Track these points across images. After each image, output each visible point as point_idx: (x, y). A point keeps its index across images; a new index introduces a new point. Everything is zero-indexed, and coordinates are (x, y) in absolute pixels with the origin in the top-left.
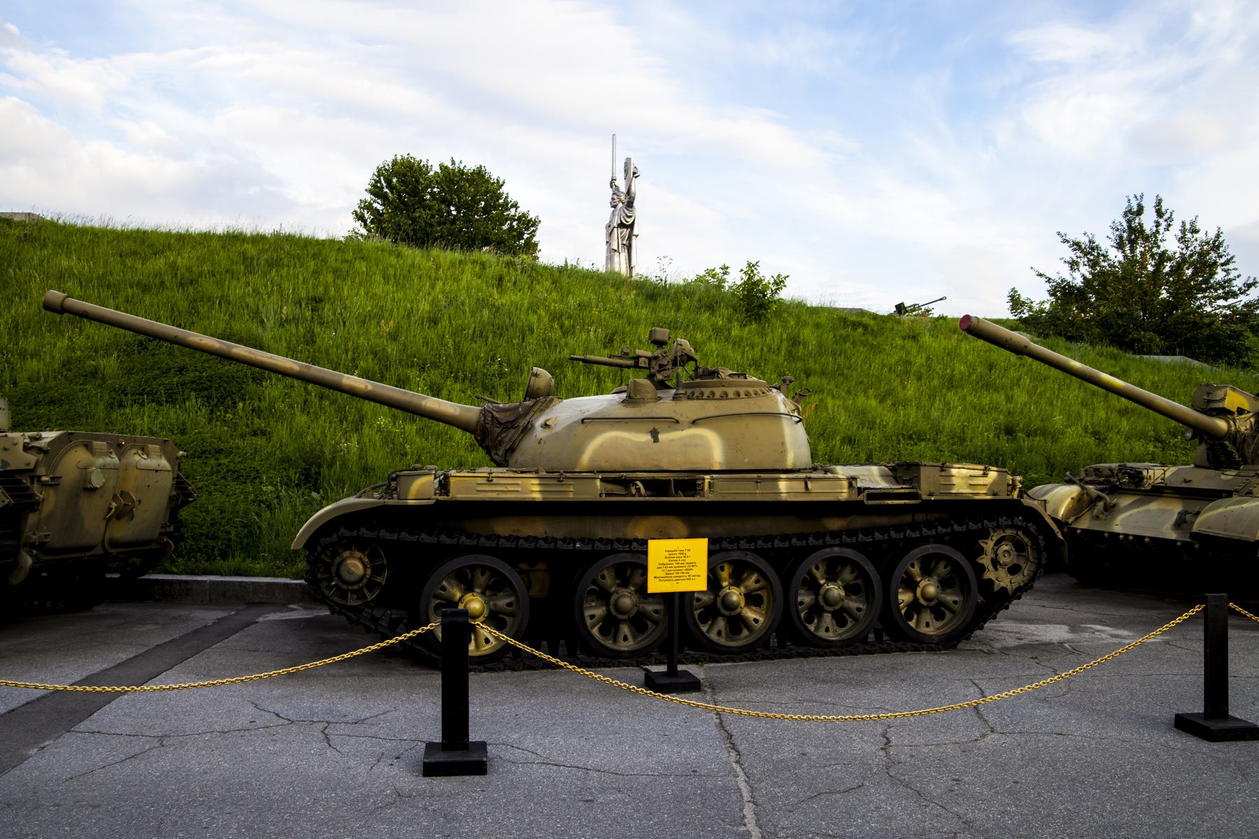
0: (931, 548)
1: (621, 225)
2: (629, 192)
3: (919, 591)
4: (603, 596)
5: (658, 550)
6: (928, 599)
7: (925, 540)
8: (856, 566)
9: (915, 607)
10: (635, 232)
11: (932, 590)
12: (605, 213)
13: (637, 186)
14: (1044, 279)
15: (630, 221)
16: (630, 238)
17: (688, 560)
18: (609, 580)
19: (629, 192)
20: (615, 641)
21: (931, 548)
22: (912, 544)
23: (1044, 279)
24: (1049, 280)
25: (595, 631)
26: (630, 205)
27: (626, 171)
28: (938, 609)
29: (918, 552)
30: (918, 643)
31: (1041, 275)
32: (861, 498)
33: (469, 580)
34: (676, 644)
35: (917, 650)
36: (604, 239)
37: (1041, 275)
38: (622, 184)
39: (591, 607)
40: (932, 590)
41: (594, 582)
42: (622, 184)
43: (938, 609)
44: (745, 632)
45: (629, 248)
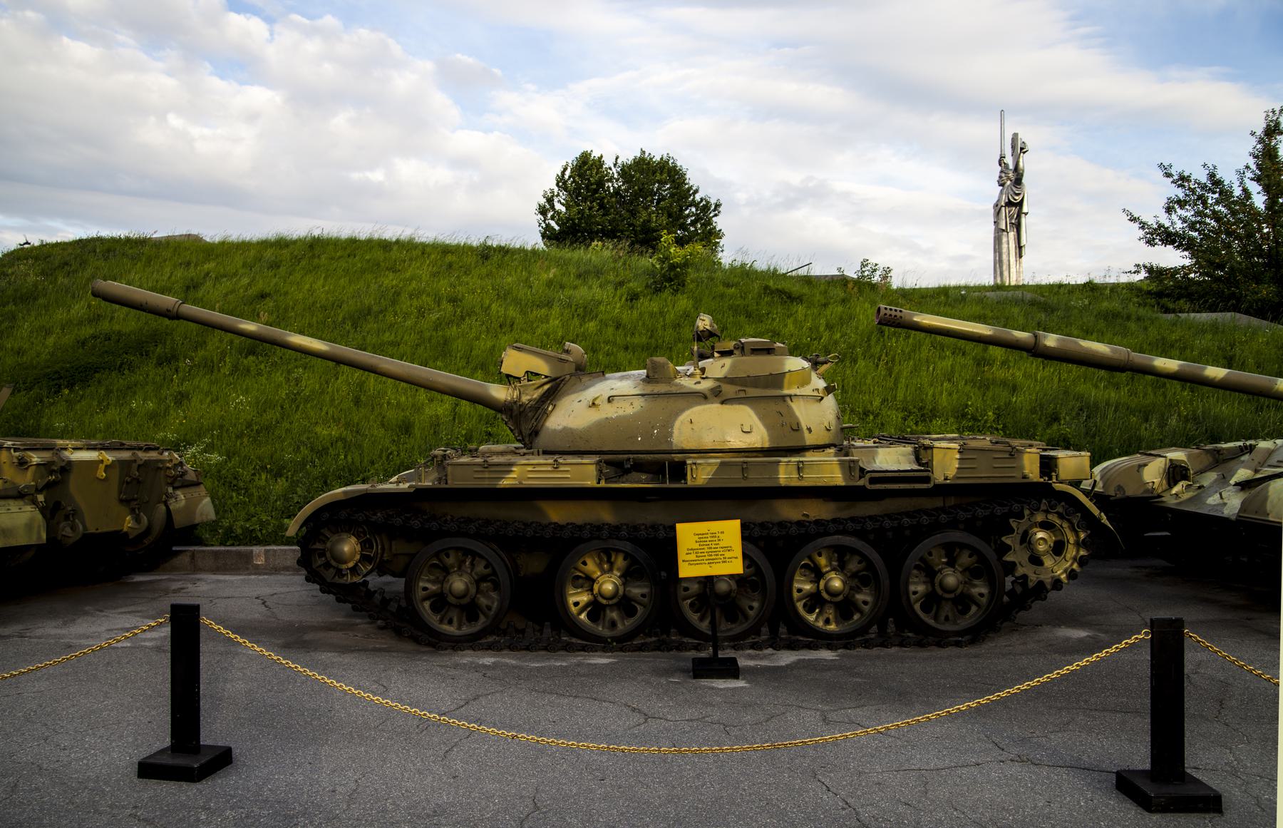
0: (956, 536)
1: (1009, 204)
2: (1016, 168)
3: (822, 583)
4: (930, 573)
5: (688, 534)
6: (833, 594)
7: (953, 525)
8: (974, 551)
9: (815, 601)
10: (1025, 210)
11: (837, 584)
12: (993, 192)
13: (1025, 161)
14: (1137, 225)
15: (1018, 198)
16: (1019, 217)
17: (722, 544)
18: (939, 559)
19: (1016, 168)
20: (936, 618)
21: (956, 536)
22: (936, 527)
23: (1137, 225)
24: (1143, 225)
25: (917, 607)
26: (1018, 181)
27: (1013, 147)
28: (963, 601)
29: (938, 538)
30: (928, 638)
31: (1133, 219)
32: (861, 483)
33: (473, 565)
34: (683, 631)
35: (921, 645)
36: (992, 220)
37: (1133, 219)
38: (1009, 161)
39: (915, 583)
40: (837, 584)
41: (810, 558)
42: (1009, 161)
43: (845, 607)
44: (974, 608)
45: (1018, 226)
